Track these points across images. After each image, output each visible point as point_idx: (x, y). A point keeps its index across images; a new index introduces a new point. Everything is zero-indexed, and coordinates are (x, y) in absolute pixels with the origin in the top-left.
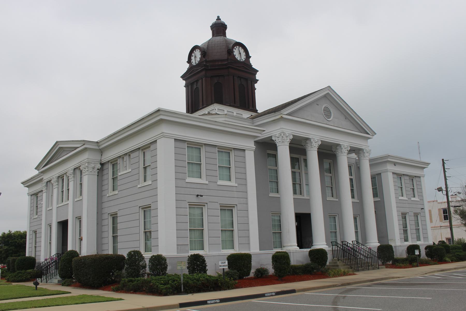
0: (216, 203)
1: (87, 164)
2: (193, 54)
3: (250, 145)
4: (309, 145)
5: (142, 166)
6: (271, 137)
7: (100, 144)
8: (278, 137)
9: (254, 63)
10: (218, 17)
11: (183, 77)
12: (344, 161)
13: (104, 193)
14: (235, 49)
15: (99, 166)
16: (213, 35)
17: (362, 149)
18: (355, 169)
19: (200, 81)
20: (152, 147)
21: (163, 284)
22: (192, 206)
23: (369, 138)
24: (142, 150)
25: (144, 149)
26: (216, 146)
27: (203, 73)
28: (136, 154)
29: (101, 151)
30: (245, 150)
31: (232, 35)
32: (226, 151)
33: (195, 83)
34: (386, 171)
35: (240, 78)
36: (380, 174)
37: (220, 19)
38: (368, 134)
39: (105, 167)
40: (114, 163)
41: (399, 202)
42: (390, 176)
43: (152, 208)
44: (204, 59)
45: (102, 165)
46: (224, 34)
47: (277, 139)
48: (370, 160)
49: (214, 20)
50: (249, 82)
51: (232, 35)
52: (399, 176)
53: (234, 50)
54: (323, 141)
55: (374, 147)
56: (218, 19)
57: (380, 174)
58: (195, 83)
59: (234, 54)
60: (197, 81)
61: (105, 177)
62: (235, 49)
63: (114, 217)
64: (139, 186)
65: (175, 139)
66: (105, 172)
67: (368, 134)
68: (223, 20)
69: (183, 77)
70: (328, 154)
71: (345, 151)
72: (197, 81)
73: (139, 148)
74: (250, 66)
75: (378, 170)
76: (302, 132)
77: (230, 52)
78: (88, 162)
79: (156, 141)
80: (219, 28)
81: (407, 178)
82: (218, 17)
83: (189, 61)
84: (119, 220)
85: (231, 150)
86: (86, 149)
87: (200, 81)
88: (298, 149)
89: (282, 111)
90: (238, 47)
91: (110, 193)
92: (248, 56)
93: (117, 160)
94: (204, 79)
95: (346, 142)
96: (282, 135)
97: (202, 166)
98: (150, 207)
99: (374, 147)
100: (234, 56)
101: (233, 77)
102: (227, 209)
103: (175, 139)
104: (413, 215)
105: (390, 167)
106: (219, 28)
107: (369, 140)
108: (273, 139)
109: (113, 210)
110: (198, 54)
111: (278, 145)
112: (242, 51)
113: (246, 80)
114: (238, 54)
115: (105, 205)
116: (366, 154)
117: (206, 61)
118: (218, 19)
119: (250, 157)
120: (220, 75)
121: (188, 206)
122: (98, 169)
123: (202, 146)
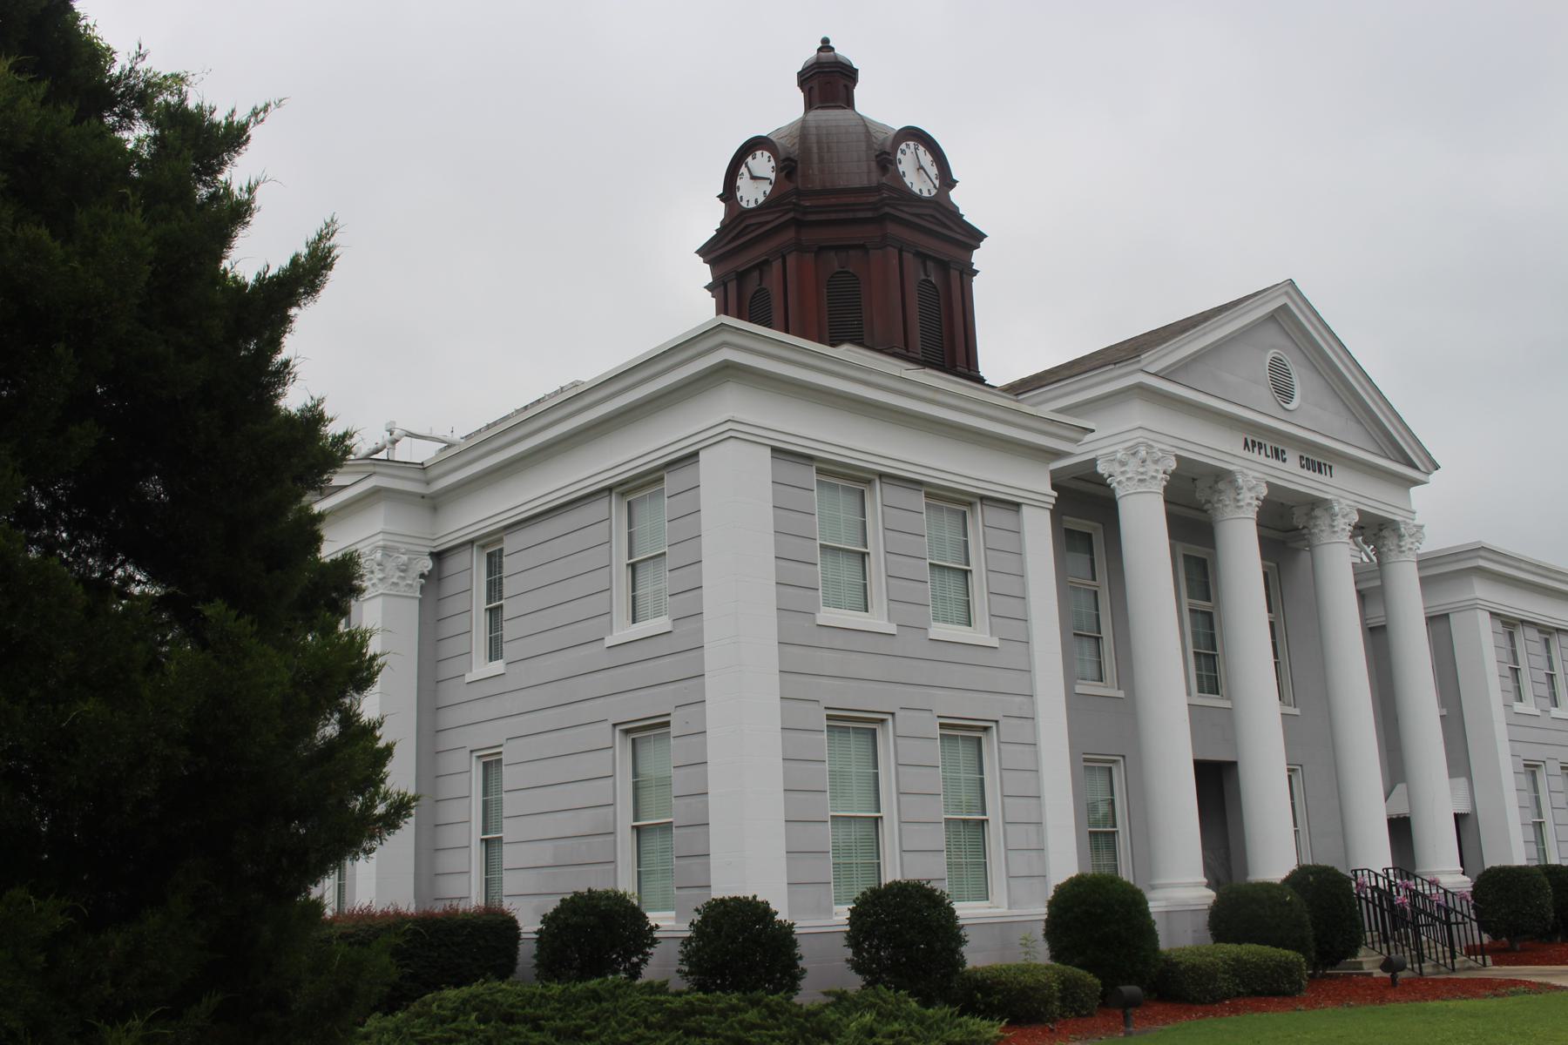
0: (927, 714)
1: (379, 555)
2: (743, 169)
3: (1035, 484)
4: (1227, 498)
5: (621, 560)
6: (1094, 461)
7: (433, 473)
8: (1123, 464)
9: (968, 201)
10: (825, 41)
11: (706, 252)
12: (1338, 559)
13: (447, 670)
14: (903, 152)
15: (427, 564)
16: (809, 105)
17: (1393, 521)
18: (1372, 591)
19: (777, 265)
20: (672, 482)
21: (662, 1028)
22: (843, 723)
23: (1416, 483)
24: (623, 494)
25: (634, 488)
26: (920, 483)
27: (789, 235)
28: (598, 509)
29: (434, 503)
30: (1018, 505)
31: (879, 103)
32: (956, 502)
33: (756, 274)
34: (1473, 607)
35: (923, 257)
36: (1447, 615)
37: (832, 49)
38: (1416, 468)
39: (453, 564)
40: (491, 547)
41: (1516, 721)
42: (1484, 618)
43: (674, 730)
44: (792, 186)
45: (438, 556)
46: (849, 103)
47: (1117, 469)
48: (1423, 563)
49: (809, 52)
50: (954, 274)
51: (879, 103)
52: (1510, 625)
53: (899, 155)
54: (1248, 483)
55: (1437, 515)
56: (826, 45)
57: (1447, 615)
58: (756, 274)
59: (901, 168)
60: (762, 266)
61: (451, 607)
62: (903, 152)
63: (491, 766)
64: (609, 641)
65: (775, 450)
66: (451, 586)
67: (1415, 467)
68: (842, 50)
69: (706, 252)
70: (1287, 530)
71: (1344, 524)
72: (762, 266)
73: (609, 489)
74: (954, 214)
75: (1445, 599)
76: (1214, 447)
77: (885, 160)
78: (384, 548)
79: (696, 454)
80: (828, 80)
81: (1532, 634)
82: (825, 41)
83: (729, 193)
84: (510, 776)
85: (970, 504)
86: (376, 494)
87: (777, 265)
88: (1192, 510)
89: (1146, 357)
90: (911, 144)
91: (482, 668)
92: (947, 181)
93: (501, 540)
94: (791, 260)
95: (1347, 495)
96: (1143, 453)
97: (872, 563)
98: (667, 724)
99: (1437, 515)
100: (899, 177)
101: (900, 251)
102: (966, 735)
103: (775, 450)
104: (1559, 772)
105: (1484, 593)
106: (828, 80)
107: (1413, 490)
108: (1102, 468)
109: (484, 737)
110: (762, 164)
111: (1119, 493)
112: (926, 159)
113: (944, 266)
114: (915, 175)
115: (449, 718)
116: (1407, 542)
117: (799, 193)
118: (826, 45)
119: (1038, 529)
120: (842, 241)
121: (825, 723)
122: (422, 576)
123: (869, 482)
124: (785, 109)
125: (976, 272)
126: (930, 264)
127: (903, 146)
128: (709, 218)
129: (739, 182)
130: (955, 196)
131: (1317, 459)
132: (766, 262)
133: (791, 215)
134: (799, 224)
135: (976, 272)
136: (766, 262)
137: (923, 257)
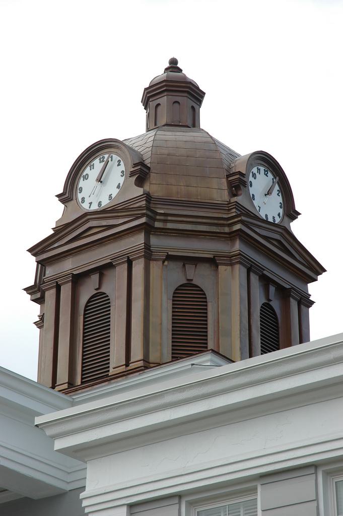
10: (174, 62)
19: (122, 270)
27: (139, 240)
33: (95, 277)
37: (180, 70)
46: (194, 122)
50: (294, 304)
51: (230, 124)
60: (102, 270)
62: (254, 176)
77: (238, 183)
80: (173, 96)
82: (174, 62)
83: (67, 196)
87: (121, 271)
92: (292, 214)
94: (138, 268)
101: (41, 285)
106: (173, 96)
113: (284, 293)
124: (131, 124)
125: (312, 303)
126: (272, 289)
127: (255, 170)
128: (47, 217)
129: (82, 183)
130: (297, 228)
131: (82, 317)
132: (110, 266)
133: (143, 220)
134: (148, 229)
135: (312, 303)
136: (110, 266)
137: (266, 281)
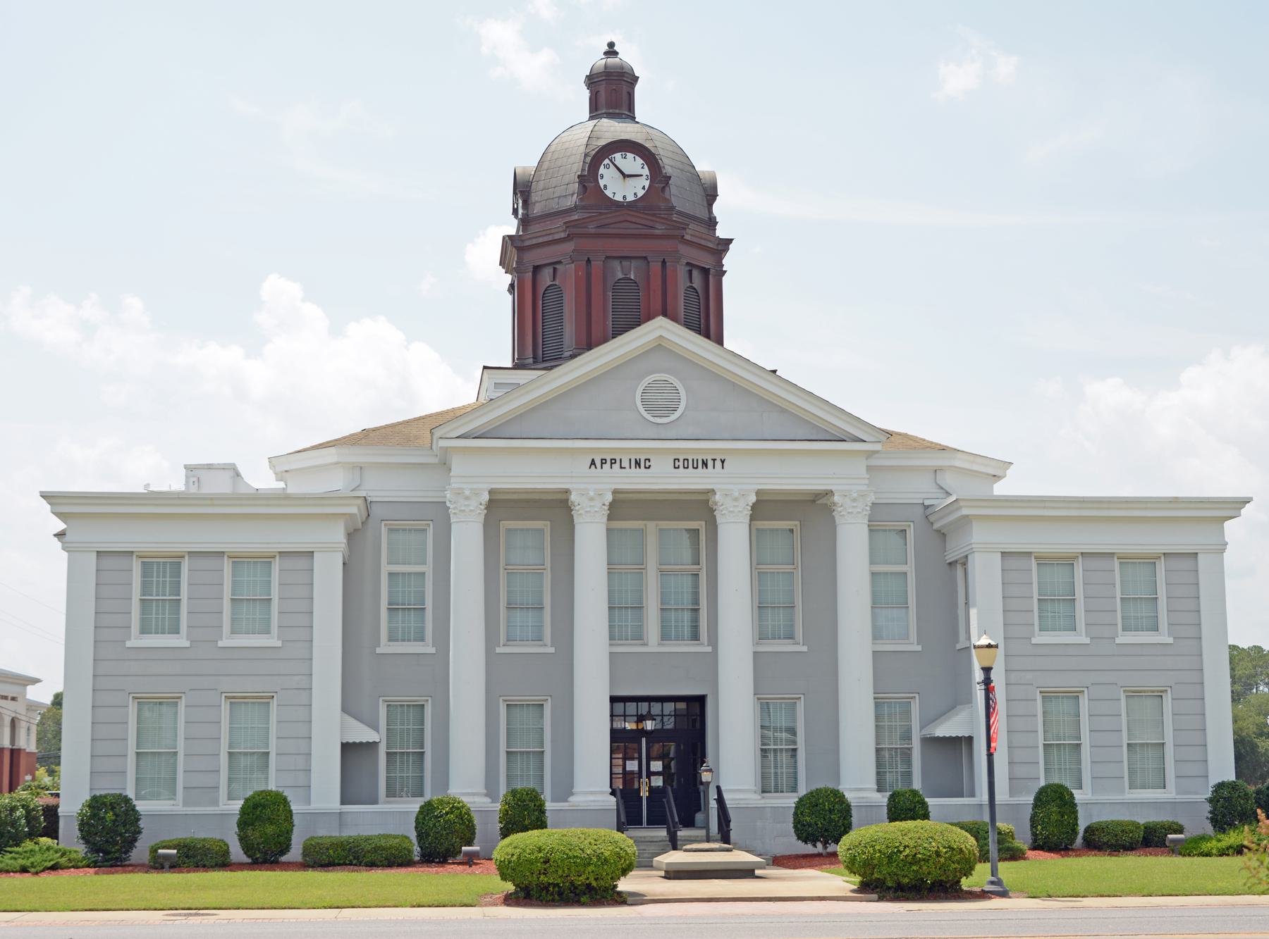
37: (616, 53)
68: (628, 56)
113: (705, 272)
